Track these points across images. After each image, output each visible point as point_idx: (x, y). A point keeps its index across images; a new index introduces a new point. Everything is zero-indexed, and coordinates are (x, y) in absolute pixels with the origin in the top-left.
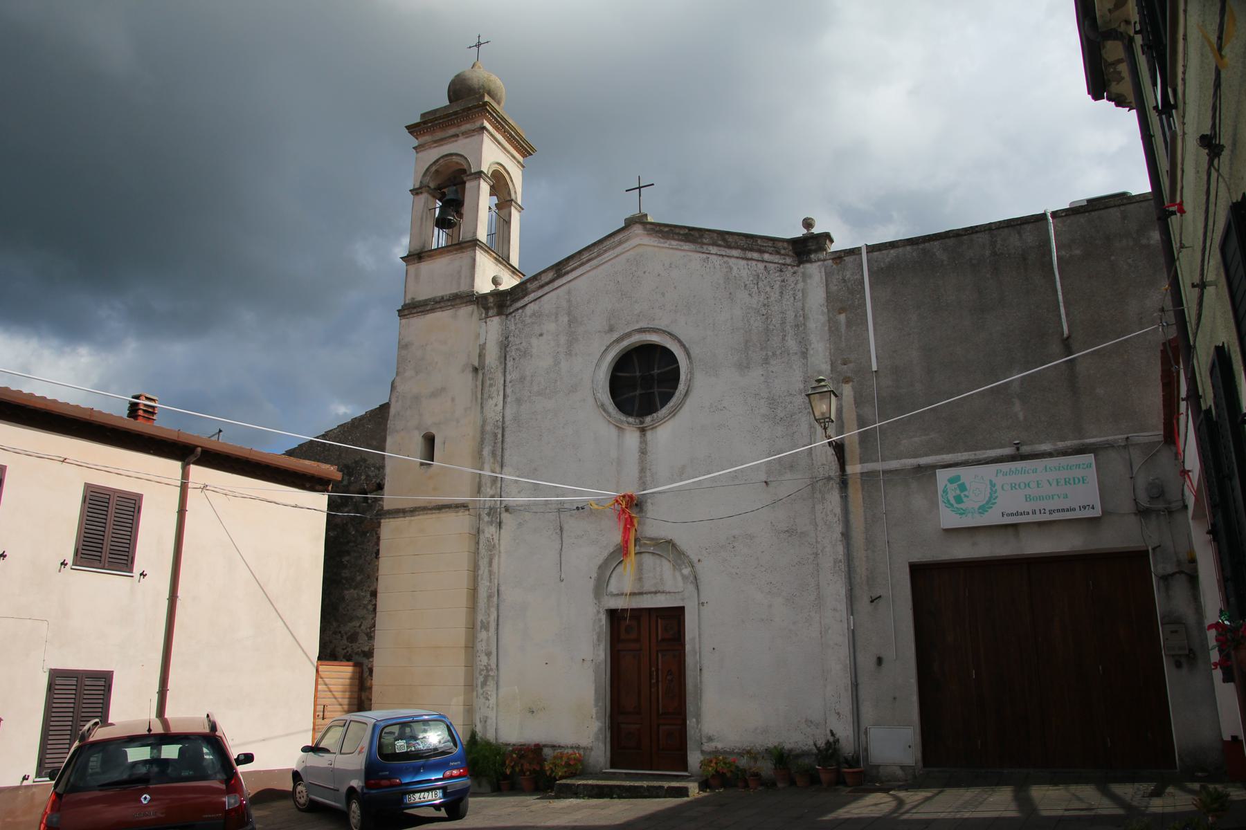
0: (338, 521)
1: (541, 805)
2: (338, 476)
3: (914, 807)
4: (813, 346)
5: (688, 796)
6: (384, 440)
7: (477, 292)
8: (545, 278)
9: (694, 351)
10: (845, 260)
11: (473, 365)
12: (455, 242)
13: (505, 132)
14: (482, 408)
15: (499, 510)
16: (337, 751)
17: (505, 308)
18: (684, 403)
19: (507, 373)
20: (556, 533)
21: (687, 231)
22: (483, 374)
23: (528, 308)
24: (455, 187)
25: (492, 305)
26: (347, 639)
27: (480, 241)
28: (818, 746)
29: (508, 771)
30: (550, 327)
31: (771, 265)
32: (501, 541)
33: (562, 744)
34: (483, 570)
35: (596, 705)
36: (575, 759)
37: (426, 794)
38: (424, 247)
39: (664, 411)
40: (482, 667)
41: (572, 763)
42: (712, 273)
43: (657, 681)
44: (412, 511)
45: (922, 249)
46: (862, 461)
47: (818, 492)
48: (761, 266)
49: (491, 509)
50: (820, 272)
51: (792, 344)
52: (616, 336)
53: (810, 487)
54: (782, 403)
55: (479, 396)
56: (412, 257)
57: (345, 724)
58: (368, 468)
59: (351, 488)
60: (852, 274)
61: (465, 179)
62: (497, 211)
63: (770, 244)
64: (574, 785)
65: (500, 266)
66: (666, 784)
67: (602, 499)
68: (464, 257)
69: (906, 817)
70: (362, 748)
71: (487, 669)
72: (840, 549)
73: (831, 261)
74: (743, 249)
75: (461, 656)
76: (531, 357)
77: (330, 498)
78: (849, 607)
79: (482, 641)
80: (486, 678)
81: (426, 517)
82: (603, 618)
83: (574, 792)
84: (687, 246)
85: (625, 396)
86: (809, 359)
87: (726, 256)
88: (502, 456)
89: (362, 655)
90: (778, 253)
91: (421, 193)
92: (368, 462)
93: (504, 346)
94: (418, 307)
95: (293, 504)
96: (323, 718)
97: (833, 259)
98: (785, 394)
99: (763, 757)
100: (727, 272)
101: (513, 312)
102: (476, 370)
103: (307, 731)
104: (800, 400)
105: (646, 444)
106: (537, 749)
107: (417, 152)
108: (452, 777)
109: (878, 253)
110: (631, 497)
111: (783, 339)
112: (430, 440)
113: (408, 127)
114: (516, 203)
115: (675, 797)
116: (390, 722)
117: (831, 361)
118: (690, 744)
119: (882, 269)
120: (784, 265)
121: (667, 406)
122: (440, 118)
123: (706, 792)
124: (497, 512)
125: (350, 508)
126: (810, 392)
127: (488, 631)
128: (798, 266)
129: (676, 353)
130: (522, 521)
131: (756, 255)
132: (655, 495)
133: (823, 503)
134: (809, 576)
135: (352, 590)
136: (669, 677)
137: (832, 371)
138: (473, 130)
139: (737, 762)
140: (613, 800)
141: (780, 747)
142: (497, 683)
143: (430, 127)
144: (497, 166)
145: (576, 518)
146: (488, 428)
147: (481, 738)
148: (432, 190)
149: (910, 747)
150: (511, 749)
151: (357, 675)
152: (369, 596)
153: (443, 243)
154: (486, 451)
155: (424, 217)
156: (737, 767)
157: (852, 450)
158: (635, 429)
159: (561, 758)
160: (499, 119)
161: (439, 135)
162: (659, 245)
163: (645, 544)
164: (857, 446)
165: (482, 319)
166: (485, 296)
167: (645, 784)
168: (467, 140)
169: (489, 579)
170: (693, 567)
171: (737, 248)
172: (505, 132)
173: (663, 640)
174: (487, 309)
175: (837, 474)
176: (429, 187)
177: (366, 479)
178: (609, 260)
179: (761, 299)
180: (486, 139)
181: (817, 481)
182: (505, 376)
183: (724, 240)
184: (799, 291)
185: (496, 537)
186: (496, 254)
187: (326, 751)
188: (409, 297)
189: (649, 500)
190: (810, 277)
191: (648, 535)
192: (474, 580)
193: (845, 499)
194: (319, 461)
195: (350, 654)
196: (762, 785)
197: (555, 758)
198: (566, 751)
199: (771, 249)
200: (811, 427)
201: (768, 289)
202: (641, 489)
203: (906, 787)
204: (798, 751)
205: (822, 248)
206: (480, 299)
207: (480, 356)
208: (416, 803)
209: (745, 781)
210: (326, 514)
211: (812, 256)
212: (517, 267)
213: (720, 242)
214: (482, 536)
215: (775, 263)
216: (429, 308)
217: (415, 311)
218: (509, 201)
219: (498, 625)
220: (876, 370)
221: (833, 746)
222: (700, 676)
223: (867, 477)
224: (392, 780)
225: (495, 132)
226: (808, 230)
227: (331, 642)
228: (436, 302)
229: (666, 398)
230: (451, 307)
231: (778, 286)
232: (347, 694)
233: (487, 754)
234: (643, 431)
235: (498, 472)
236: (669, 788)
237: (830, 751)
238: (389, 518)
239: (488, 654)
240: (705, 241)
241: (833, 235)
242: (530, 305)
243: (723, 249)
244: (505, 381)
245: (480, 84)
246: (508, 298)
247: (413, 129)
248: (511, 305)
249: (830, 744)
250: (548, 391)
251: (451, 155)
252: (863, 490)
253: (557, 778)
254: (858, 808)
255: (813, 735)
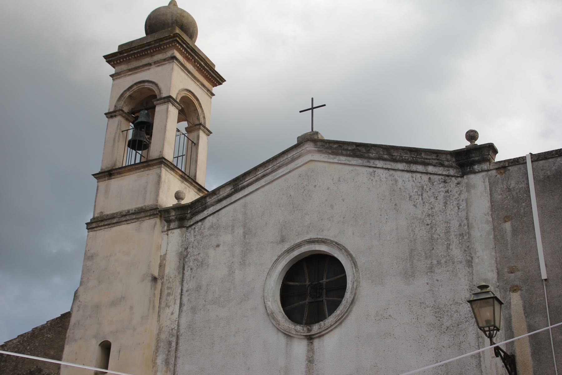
4: (478, 254)
9: (361, 261)
10: (509, 170)
13: (195, 62)
14: (159, 316)
18: (350, 311)
19: (185, 282)
21: (355, 147)
23: (207, 221)
27: (166, 160)
30: (226, 238)
31: (435, 176)
38: (115, 165)
39: (330, 320)
48: (425, 178)
50: (484, 182)
51: (457, 252)
52: (287, 246)
54: (448, 311)
55: (157, 304)
56: (103, 174)
60: (517, 183)
65: (186, 183)
74: (408, 162)
76: (208, 266)
84: (354, 161)
86: (474, 268)
87: (391, 169)
88: (175, 365)
90: (442, 165)
91: (115, 116)
93: (183, 257)
94: (106, 220)
97: (497, 169)
98: (451, 303)
101: (193, 224)
102: (155, 279)
105: (313, 353)
109: (544, 161)
111: (448, 248)
112: (106, 347)
114: (204, 127)
119: (548, 177)
120: (448, 176)
121: (334, 315)
128: (462, 176)
131: (420, 168)
137: (498, 279)
146: (163, 336)
154: (160, 360)
155: (117, 138)
160: (189, 50)
164: (530, 358)
165: (165, 232)
166: (167, 211)
171: (402, 161)
174: (169, 222)
176: (122, 110)
179: (426, 209)
182: (182, 285)
183: (390, 154)
188: (98, 211)
190: (474, 187)
201: (432, 200)
215: (439, 175)
217: (102, 224)
220: (546, 278)
225: (185, 61)
230: (136, 220)
231: (442, 196)
234: (310, 338)
241: (497, 146)
242: (208, 218)
243: (388, 163)
244: (182, 290)
245: (174, 19)
246: (189, 211)
247: (110, 59)
250: (222, 299)
251: (144, 82)
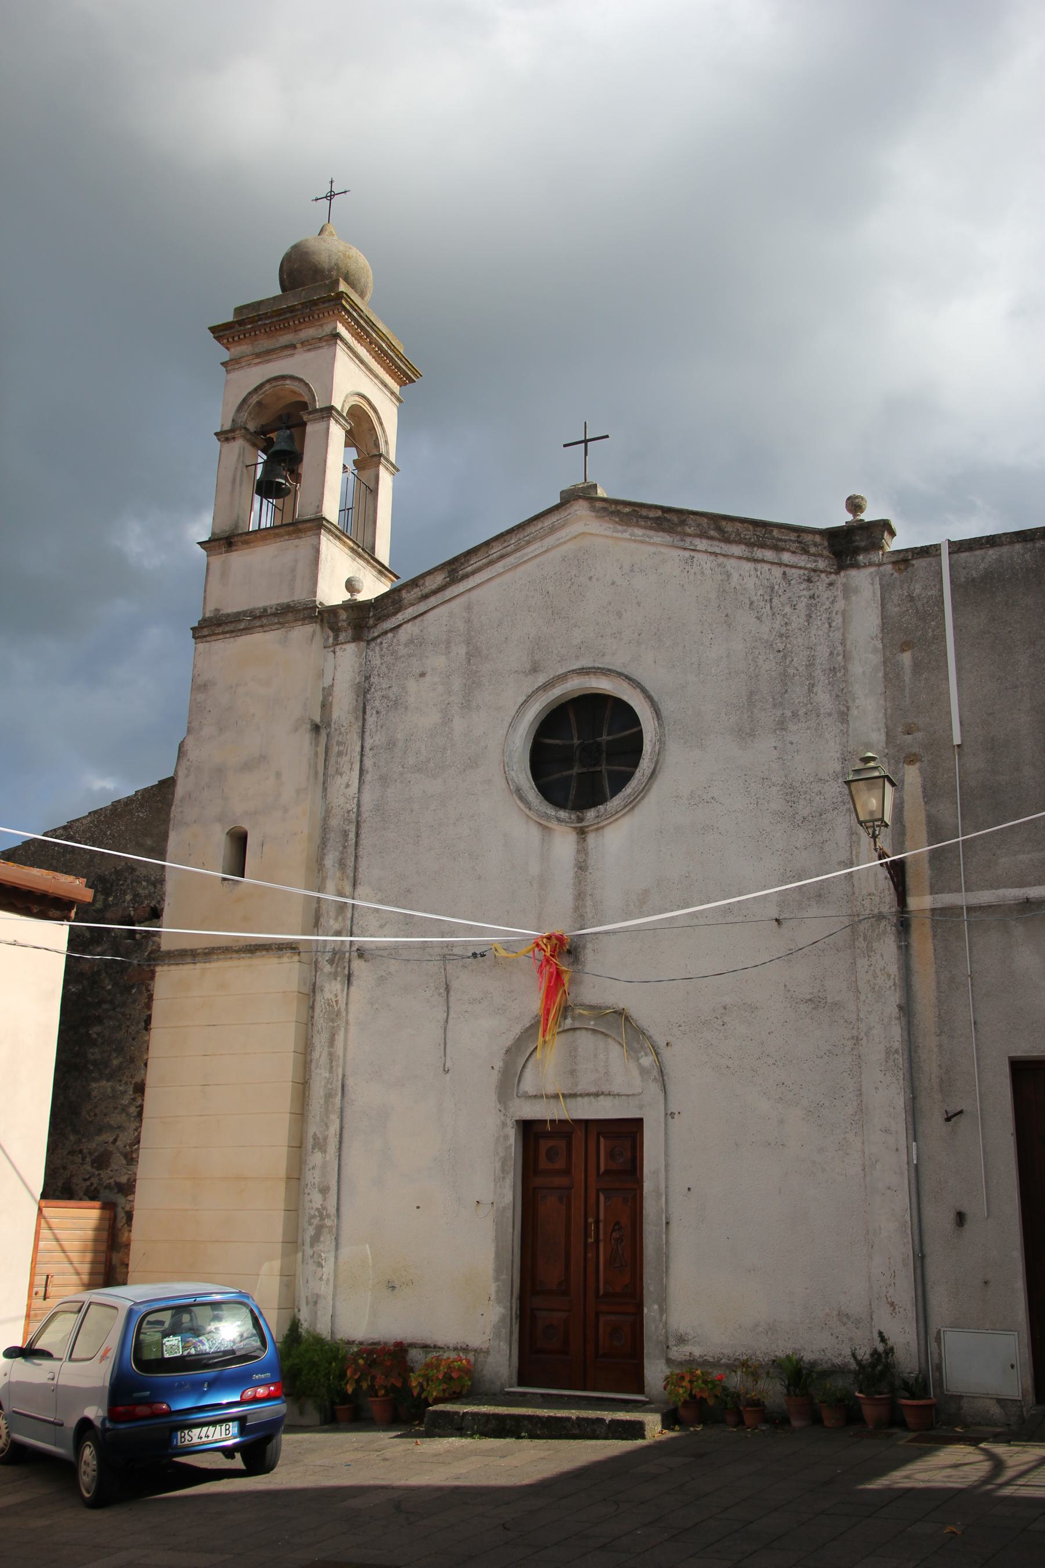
0: (86, 967)
1: (401, 1448)
2: (87, 895)
3: (1023, 1474)
5: (643, 1437)
6: (165, 837)
7: (321, 603)
8: (432, 583)
9: (668, 707)
10: (913, 565)
11: (312, 721)
12: (288, 520)
13: (371, 343)
14: (325, 789)
15: (347, 955)
16: (65, 1355)
17: (366, 630)
18: (648, 790)
19: (367, 734)
20: (440, 994)
22: (328, 736)
23: (402, 630)
24: (288, 431)
25: (345, 624)
26: (93, 1162)
27: (328, 521)
28: (859, 1358)
29: (350, 1389)
31: (794, 570)
32: (350, 1006)
33: (439, 1344)
34: (320, 1054)
35: (497, 1279)
36: (459, 1369)
37: (211, 1429)
38: (237, 526)
40: (312, 1212)
41: (454, 1375)
42: (699, 582)
43: (597, 1241)
44: (205, 954)
45: (1040, 550)
46: (934, 890)
47: (861, 939)
48: (777, 572)
49: (335, 953)
50: (872, 584)
51: (823, 698)
52: (541, 679)
53: (848, 930)
54: (806, 792)
57: (82, 1310)
58: (138, 882)
59: (109, 915)
61: (305, 418)
62: (356, 472)
63: (793, 536)
64: (457, 1413)
65: (360, 561)
66: (608, 1416)
67: (514, 941)
68: (300, 546)
69: (1007, 1491)
70: (107, 1350)
71: (321, 1215)
72: (896, 1031)
73: (890, 567)
74: (750, 545)
75: (280, 1192)
77: (71, 927)
78: (910, 1127)
79: (313, 1168)
80: (319, 1229)
81: (229, 963)
82: (512, 1134)
83: (457, 1426)
84: (659, 537)
85: (556, 776)
86: (851, 724)
87: (721, 554)
88: (356, 869)
89: (116, 1190)
90: (805, 551)
91: (234, 438)
92: (138, 873)
93: (363, 691)
94: (226, 623)
95: (11, 940)
96: (45, 1298)
97: (894, 563)
98: (812, 779)
99: (768, 1373)
100: (722, 580)
101: (379, 636)
102: (316, 728)
103: (15, 1319)
104: (835, 789)
105: (587, 854)
106: (400, 1351)
107: (228, 372)
108: (255, 1400)
109: (967, 554)
110: (560, 939)
111: (810, 691)
112: (239, 840)
113: (213, 330)
114: (388, 460)
115: (623, 1439)
116: (157, 1306)
117: (887, 727)
118: (649, 1348)
119: (973, 580)
120: (814, 571)
121: (621, 795)
122: (266, 316)
123: (673, 1430)
124: (344, 958)
125: (105, 946)
126: (851, 778)
127: (325, 1152)
128: (837, 573)
129: (637, 710)
130: (384, 974)
131: (769, 555)
132: (601, 936)
133: (869, 956)
134: (845, 1074)
135: (104, 1083)
136: (615, 1235)
137: (887, 743)
138: (320, 339)
139: (724, 1380)
140: (520, 1440)
141: (795, 1358)
142: (337, 1239)
143: (250, 331)
144: (357, 398)
145: (472, 971)
146: (334, 822)
147: (308, 1332)
148: (251, 433)
149: (1012, 1366)
150: (356, 1349)
151: (106, 1224)
152: (131, 1093)
153: (266, 522)
156: (725, 1389)
157: (918, 877)
158: (569, 830)
159: (438, 1367)
160: (362, 322)
161: (265, 344)
162: (615, 535)
163: (581, 1015)
164: (927, 866)
165: (329, 647)
166: (333, 610)
167: (573, 1414)
168: (311, 354)
169: (328, 1066)
170: (657, 1054)
171: (739, 542)
172: (371, 343)
173: (607, 1172)
174: (336, 630)
175: (894, 910)
176: (246, 429)
177: (133, 900)
178: (536, 556)
179: (777, 626)
180: (341, 354)
181: (860, 921)
182: (363, 739)
183: (719, 529)
184: (836, 614)
185: (342, 999)
186: (354, 542)
187: (45, 1355)
189: (589, 945)
190: (856, 591)
191: (587, 1002)
192: (305, 1068)
193: (905, 950)
194: (55, 870)
195: (96, 1189)
196: (766, 1421)
197: (428, 1366)
198: (445, 1356)
199: (794, 546)
200: (852, 833)
201: (788, 609)
202: (578, 926)
203: (1007, 1438)
204: (825, 1366)
205: (877, 546)
206: (326, 615)
207: (323, 706)
208: (194, 1445)
209: (739, 1414)
210: (65, 955)
211: (861, 558)
212: (387, 564)
213: (712, 533)
214: (318, 997)
215: (801, 568)
216: (242, 626)
217: (220, 629)
218: (375, 455)
219: (340, 1142)
220: (959, 743)
221: (884, 1360)
222: (667, 1234)
223: (939, 914)
224: (156, 1406)
225: (356, 342)
226: (855, 515)
227: (65, 1168)
228: (255, 618)
229: (620, 781)
231: (804, 604)
232: (89, 1256)
233: (316, 1359)
234: (582, 832)
235: (348, 894)
236: (612, 1421)
237: (879, 1368)
238: (170, 965)
239: (324, 1190)
240: (688, 530)
241: (894, 524)
242: (405, 626)
243: (715, 543)
244: (362, 747)
245: (333, 261)
246: (371, 614)
248: (375, 625)
249: (879, 1355)
251: (283, 378)
252: (934, 936)
253: (430, 1400)
254: (926, 1471)
255: (851, 1339)
